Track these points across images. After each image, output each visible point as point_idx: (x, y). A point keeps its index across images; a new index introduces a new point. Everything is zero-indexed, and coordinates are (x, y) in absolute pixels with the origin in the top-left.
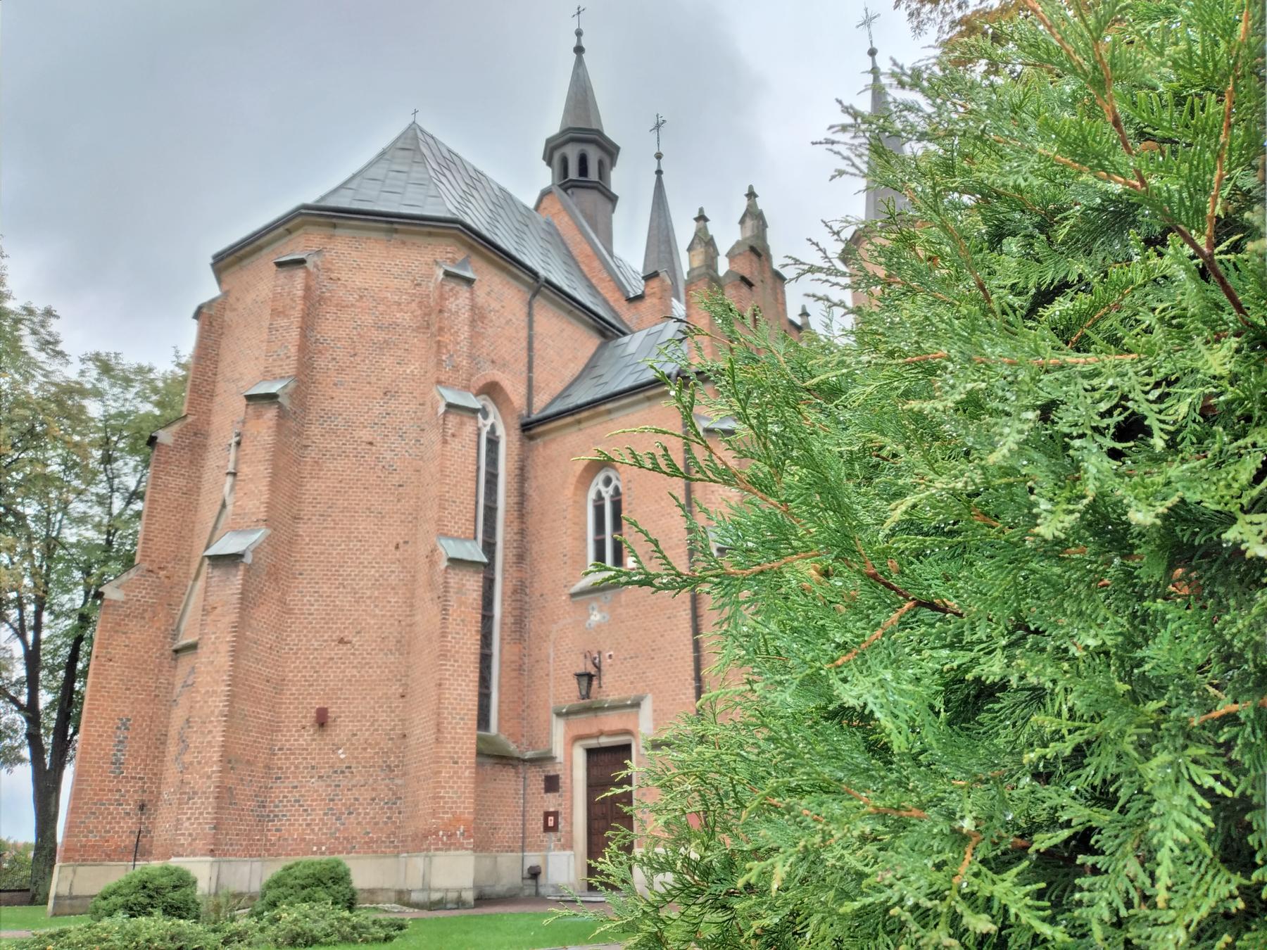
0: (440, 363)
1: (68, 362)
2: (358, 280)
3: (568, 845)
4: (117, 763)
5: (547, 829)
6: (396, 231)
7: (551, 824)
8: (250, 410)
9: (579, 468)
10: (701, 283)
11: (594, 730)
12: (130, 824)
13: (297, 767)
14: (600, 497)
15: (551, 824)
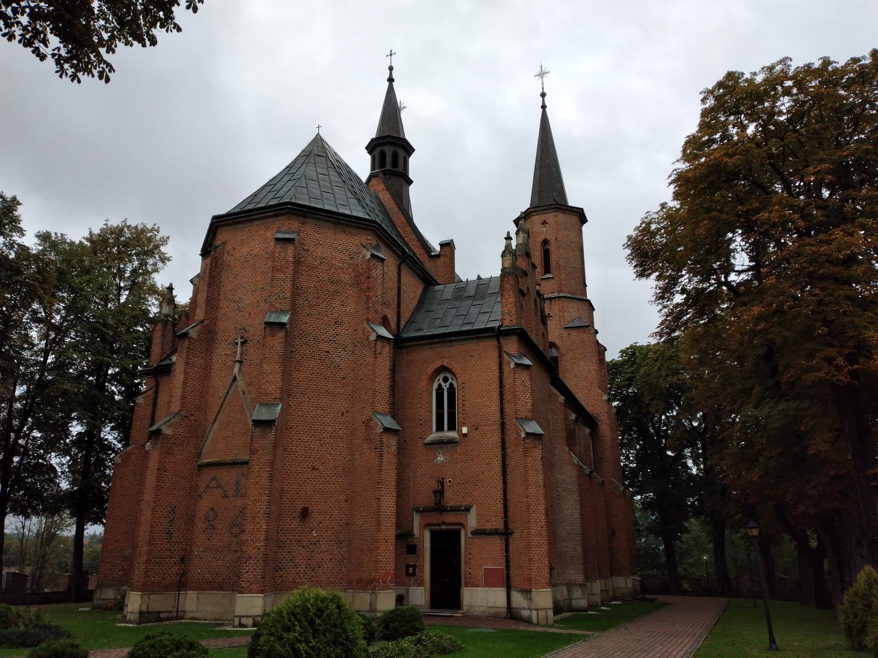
0: (368, 308)
1: (23, 235)
2: (319, 252)
3: (421, 584)
4: (169, 533)
5: (408, 574)
6: (340, 224)
7: (411, 571)
8: (267, 331)
9: (430, 370)
10: (510, 278)
11: (440, 521)
12: (175, 569)
13: (291, 541)
14: (440, 386)
15: (411, 571)
